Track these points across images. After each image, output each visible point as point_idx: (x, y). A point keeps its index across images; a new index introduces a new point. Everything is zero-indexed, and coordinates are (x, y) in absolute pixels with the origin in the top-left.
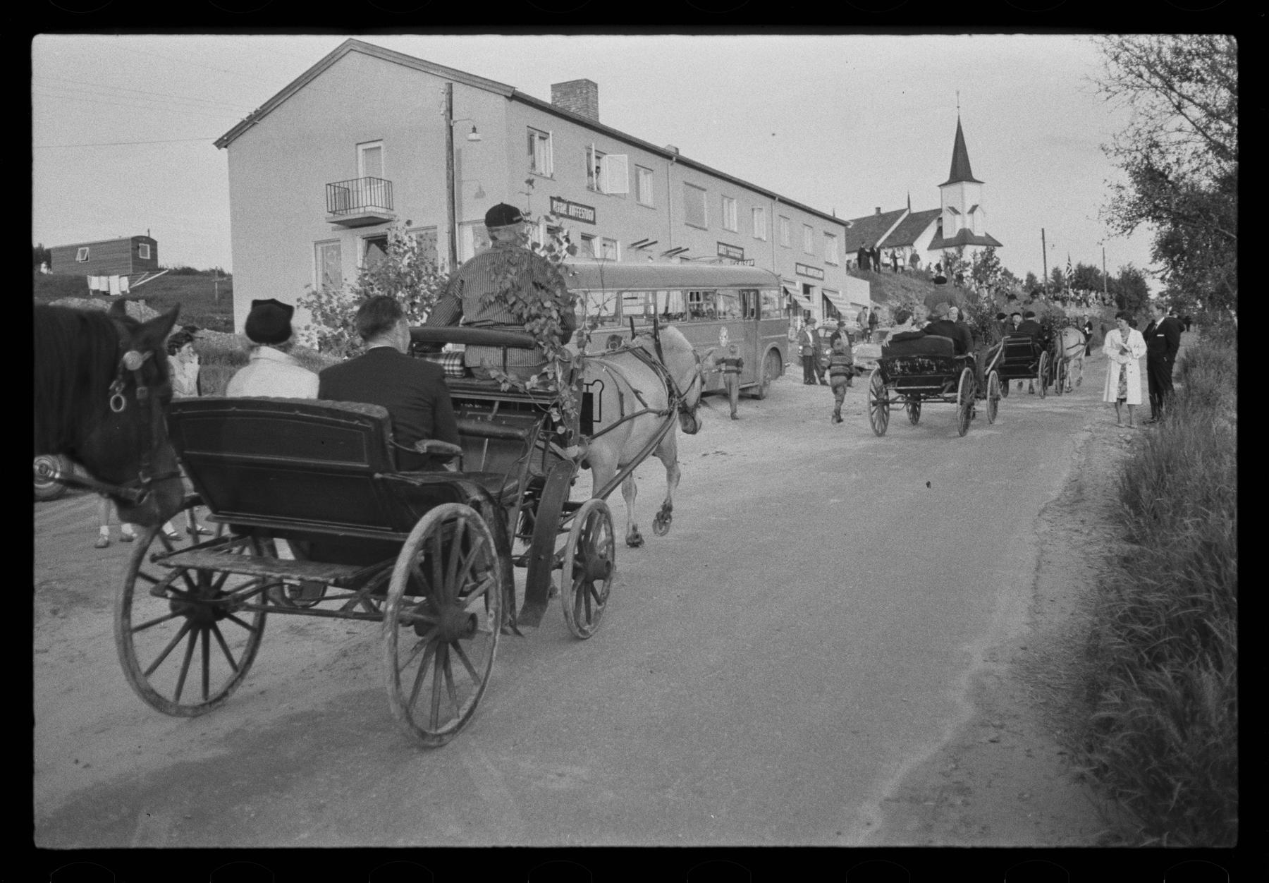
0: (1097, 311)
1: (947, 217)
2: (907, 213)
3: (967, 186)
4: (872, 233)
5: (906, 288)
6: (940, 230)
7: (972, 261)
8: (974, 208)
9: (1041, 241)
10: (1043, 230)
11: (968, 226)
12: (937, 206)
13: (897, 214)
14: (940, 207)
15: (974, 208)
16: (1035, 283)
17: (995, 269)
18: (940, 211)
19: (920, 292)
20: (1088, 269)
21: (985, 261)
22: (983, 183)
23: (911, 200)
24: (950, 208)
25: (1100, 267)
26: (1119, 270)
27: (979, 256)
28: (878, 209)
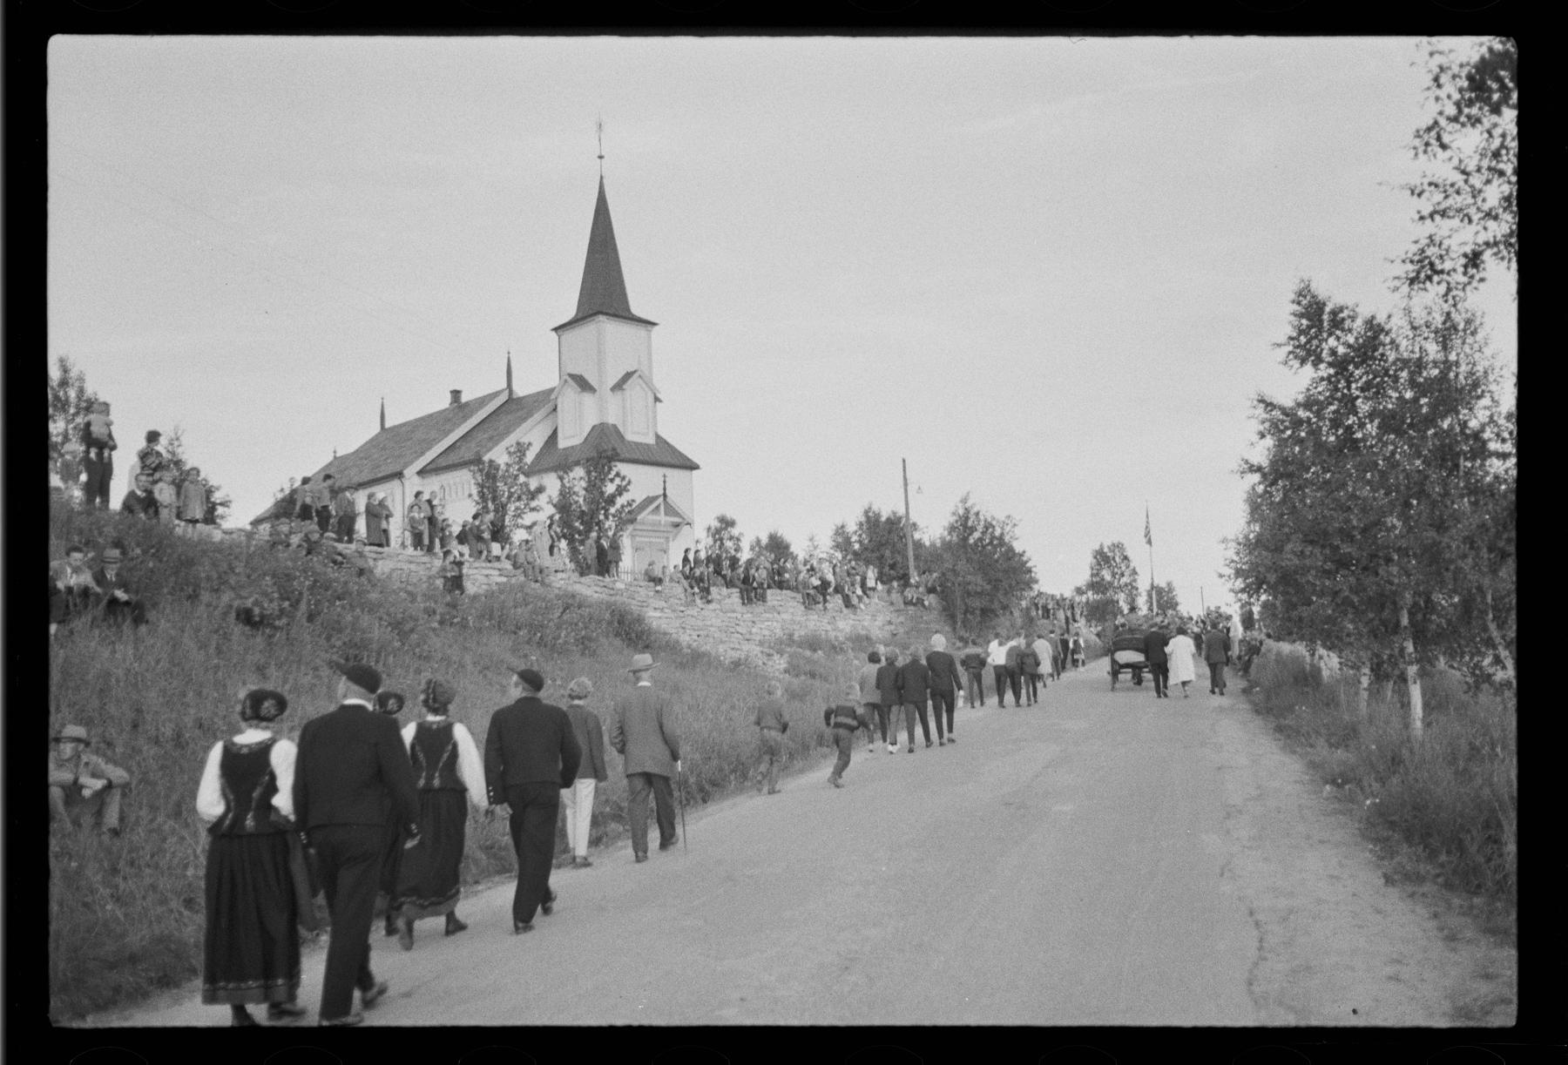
0: (880, 620)
1: (569, 399)
2: (504, 398)
3: (610, 329)
10: (904, 461)
11: (611, 420)
22: (654, 324)
23: (513, 365)
24: (571, 376)
28: (456, 394)
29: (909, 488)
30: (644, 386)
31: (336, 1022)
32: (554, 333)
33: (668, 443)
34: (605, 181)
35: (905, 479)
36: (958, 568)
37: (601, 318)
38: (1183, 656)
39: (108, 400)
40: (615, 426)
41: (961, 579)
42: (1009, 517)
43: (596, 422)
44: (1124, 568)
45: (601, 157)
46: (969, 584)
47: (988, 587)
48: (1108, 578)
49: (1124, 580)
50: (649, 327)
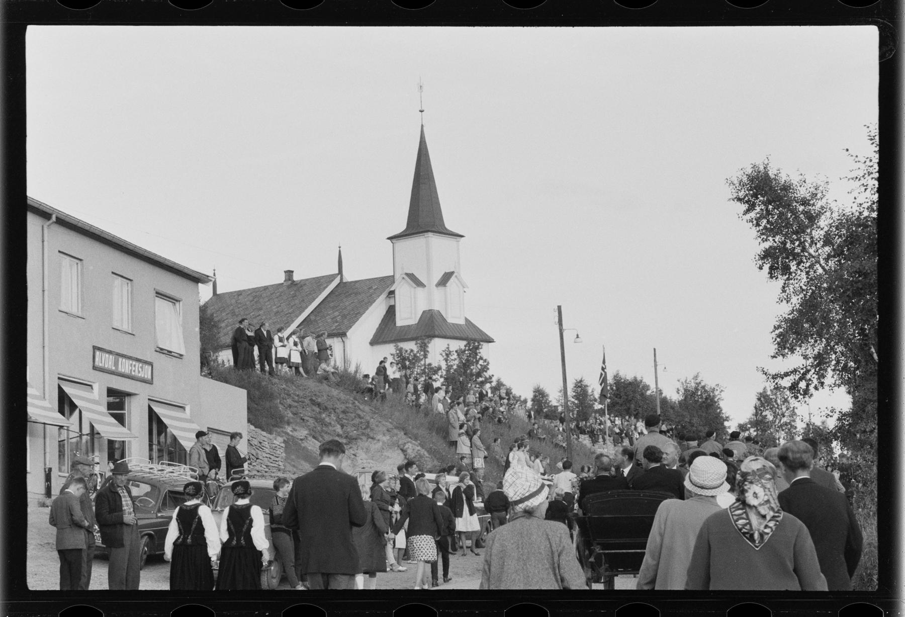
1: (403, 290)
2: (337, 281)
3: (434, 240)
5: (319, 405)
6: (391, 311)
7: (444, 366)
9: (557, 327)
10: (655, 349)
11: (436, 307)
13: (319, 283)
17: (480, 379)
18: (390, 280)
19: (344, 412)
20: (630, 383)
21: (465, 366)
22: (462, 236)
24: (407, 274)
25: (649, 380)
26: (679, 385)
27: (455, 356)
28: (289, 273)
29: (658, 367)
32: (389, 241)
34: (425, 128)
35: (655, 361)
37: (430, 234)
40: (439, 311)
42: (718, 385)
43: (427, 309)
44: (784, 409)
45: (421, 111)
48: (770, 418)
49: (784, 420)
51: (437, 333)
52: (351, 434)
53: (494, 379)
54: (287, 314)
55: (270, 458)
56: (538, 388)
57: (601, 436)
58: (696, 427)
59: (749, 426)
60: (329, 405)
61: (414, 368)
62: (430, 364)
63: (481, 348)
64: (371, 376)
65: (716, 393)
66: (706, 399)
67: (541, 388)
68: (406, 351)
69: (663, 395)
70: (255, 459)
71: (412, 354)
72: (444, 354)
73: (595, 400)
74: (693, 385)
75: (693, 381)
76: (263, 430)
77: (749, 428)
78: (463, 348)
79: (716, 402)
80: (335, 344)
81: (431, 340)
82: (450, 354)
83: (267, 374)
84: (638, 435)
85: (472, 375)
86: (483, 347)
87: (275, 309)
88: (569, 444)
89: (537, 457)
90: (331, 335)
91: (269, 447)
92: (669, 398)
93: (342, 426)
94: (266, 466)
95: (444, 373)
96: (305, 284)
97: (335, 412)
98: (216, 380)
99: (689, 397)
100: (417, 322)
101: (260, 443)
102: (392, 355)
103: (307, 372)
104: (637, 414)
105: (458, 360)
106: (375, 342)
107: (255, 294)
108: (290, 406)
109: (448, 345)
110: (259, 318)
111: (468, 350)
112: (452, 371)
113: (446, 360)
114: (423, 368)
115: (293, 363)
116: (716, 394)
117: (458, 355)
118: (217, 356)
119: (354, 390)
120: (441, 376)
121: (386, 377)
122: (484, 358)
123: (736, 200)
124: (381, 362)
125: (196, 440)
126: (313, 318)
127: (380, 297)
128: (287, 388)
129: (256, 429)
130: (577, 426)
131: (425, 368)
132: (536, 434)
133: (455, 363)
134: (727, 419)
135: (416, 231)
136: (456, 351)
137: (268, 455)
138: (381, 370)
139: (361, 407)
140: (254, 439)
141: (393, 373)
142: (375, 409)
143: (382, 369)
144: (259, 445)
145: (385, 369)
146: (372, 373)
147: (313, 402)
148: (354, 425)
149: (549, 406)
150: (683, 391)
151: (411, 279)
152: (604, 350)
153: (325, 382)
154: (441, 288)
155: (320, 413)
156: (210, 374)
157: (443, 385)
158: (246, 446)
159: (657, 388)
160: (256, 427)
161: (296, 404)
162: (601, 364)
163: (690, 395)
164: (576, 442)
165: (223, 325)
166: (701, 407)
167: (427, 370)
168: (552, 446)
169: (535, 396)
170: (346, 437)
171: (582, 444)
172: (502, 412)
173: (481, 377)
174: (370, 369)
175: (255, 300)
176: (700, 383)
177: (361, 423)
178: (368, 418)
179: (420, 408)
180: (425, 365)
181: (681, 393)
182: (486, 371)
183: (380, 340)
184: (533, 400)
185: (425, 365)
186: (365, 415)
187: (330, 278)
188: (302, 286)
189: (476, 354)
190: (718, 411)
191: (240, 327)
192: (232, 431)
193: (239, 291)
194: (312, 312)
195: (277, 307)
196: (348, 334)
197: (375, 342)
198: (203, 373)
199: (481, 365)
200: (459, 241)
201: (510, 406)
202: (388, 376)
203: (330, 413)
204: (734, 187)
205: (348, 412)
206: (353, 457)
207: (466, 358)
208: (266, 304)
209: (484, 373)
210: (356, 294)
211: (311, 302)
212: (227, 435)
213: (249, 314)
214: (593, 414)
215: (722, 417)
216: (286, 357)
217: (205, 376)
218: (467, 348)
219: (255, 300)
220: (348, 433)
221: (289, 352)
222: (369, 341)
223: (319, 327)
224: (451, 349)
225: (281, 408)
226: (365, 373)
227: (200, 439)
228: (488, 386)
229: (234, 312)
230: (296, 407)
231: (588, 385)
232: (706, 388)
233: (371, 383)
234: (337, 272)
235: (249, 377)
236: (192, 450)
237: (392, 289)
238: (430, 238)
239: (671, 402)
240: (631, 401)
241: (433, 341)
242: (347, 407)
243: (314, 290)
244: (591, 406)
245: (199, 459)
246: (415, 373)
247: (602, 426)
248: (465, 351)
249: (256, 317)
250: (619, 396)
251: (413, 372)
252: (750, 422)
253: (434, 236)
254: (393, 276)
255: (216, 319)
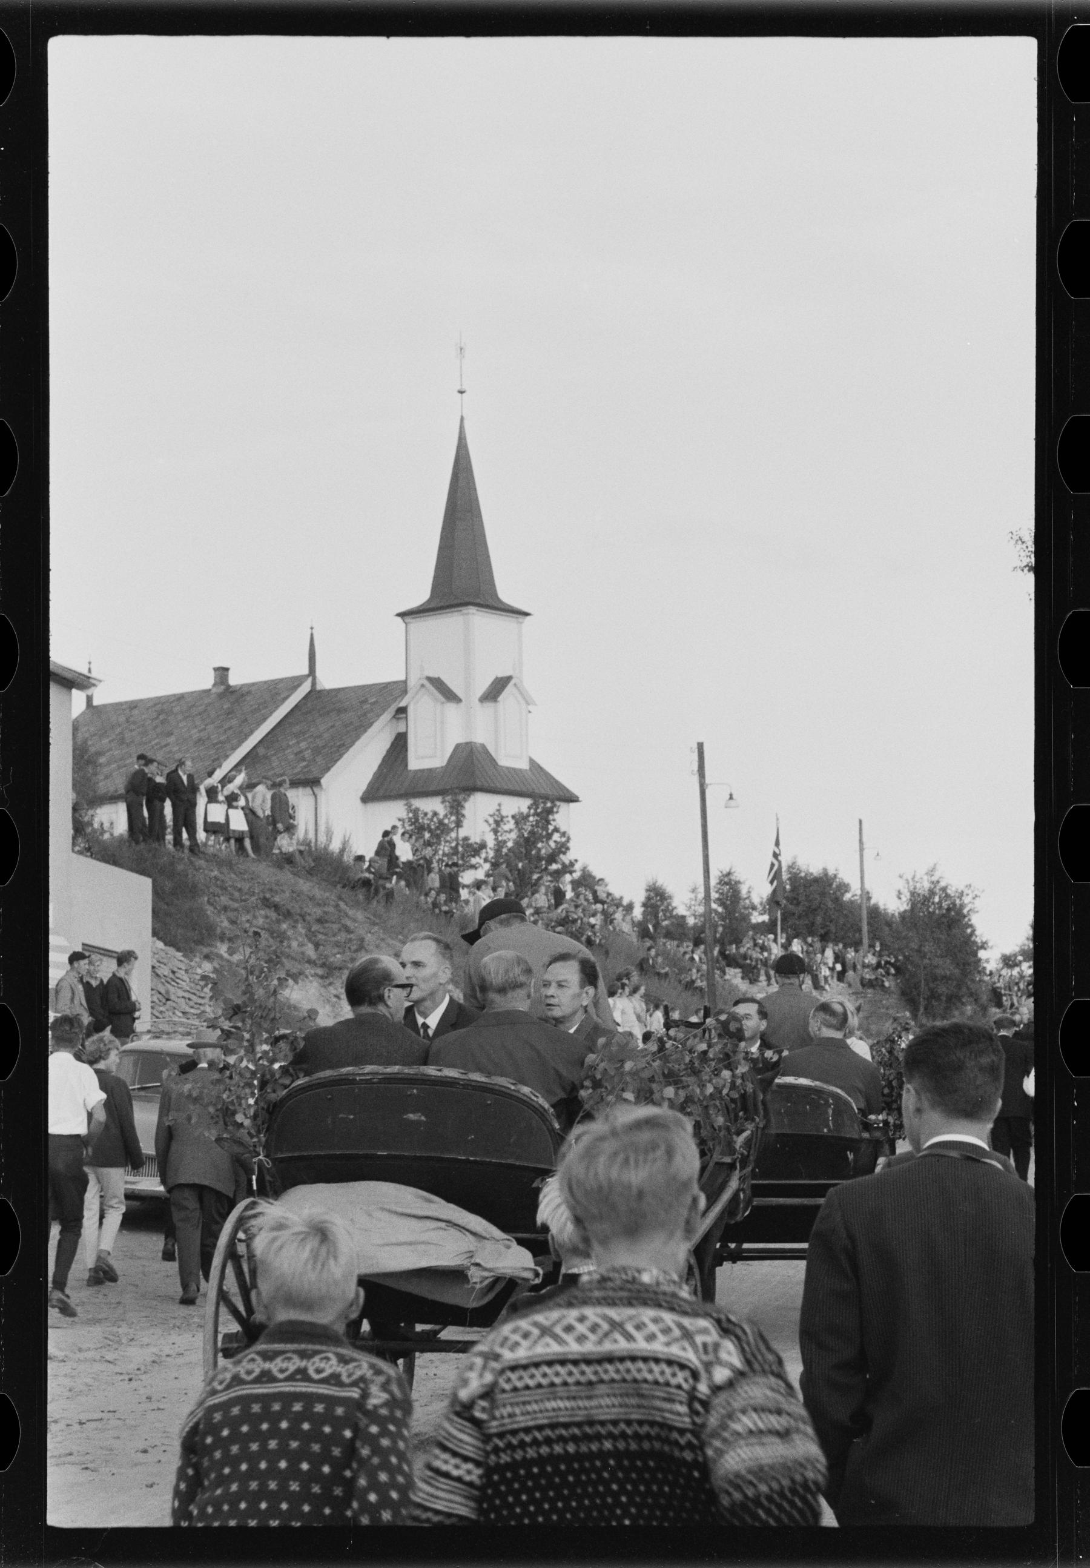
2: (306, 688)
3: (479, 620)
4: (200, 740)
5: (276, 907)
6: (400, 744)
7: (491, 842)
8: (497, 689)
9: (696, 779)
10: (860, 822)
11: (480, 737)
12: (394, 673)
13: (276, 690)
14: (403, 678)
15: (497, 689)
16: (669, 912)
17: (554, 867)
18: (400, 688)
19: (320, 921)
20: (816, 880)
21: (528, 842)
22: (527, 614)
24: (429, 679)
25: (848, 875)
26: (901, 885)
27: (510, 825)
28: (222, 672)
29: (865, 852)
30: (519, 696)
31: (508, 1303)
32: (399, 619)
33: (541, 768)
35: (861, 841)
36: (926, 949)
37: (472, 610)
38: (102, 1194)
39: (391, 826)
40: (483, 746)
41: (926, 961)
42: (969, 886)
45: (461, 392)
46: (936, 967)
47: (957, 971)
50: (521, 618)
51: (479, 783)
52: (331, 960)
53: (578, 867)
54: (217, 744)
55: (189, 999)
56: (654, 884)
57: (762, 972)
58: (930, 959)
59: (1020, 958)
60: (295, 908)
61: (439, 844)
62: (466, 839)
63: (557, 812)
64: (367, 859)
65: (966, 900)
66: (949, 910)
67: (659, 884)
68: (426, 814)
69: (873, 902)
70: (164, 1001)
71: (435, 819)
72: (491, 821)
73: (754, 908)
74: (927, 885)
75: (925, 877)
76: (178, 950)
77: (1020, 962)
78: (525, 810)
79: (965, 916)
80: (300, 799)
81: (469, 796)
82: (502, 820)
83: (186, 851)
84: (827, 970)
85: (539, 858)
86: (561, 810)
87: (195, 734)
88: (712, 985)
89: (657, 1007)
90: (295, 784)
91: (188, 980)
92: (882, 907)
93: (317, 945)
94: (183, 1013)
95: (491, 854)
96: (249, 692)
97: (304, 920)
98: (98, 859)
99: (919, 905)
100: (444, 764)
101: (173, 972)
102: (399, 820)
103: (256, 848)
104: (826, 933)
105: (516, 831)
106: (369, 797)
107: (159, 707)
108: (225, 909)
109: (499, 805)
110: (167, 749)
111: (533, 815)
112: (505, 850)
113: (495, 831)
114: (453, 844)
115: (234, 831)
116: (966, 901)
117: (517, 823)
118: (92, 816)
119: (339, 883)
120: (486, 860)
121: (393, 860)
122: (562, 830)
123: (1026, 570)
124: (386, 834)
125: (68, 967)
126: (261, 751)
127: (382, 717)
128: (221, 876)
129: (167, 948)
130: (722, 953)
131: (457, 844)
132: (653, 966)
133: (511, 838)
134: (983, 946)
135: (447, 604)
136: (513, 817)
137: (187, 995)
138: (386, 848)
139: (351, 913)
140: (162, 966)
141: (404, 852)
142: (375, 915)
143: (387, 845)
144: (171, 975)
145: (392, 845)
146: (369, 853)
147: (267, 903)
148: (337, 944)
149: (672, 916)
150: (908, 895)
151: (437, 688)
152: (777, 824)
153: (287, 866)
154: (489, 706)
155: (278, 921)
156: (89, 849)
157: (488, 875)
158: (149, 978)
159: (862, 888)
160: (166, 944)
161: (236, 905)
162: (772, 848)
163: (919, 902)
164: (719, 979)
165: (102, 760)
166: (939, 924)
167: (460, 849)
168: (680, 988)
169: (649, 898)
170: (323, 965)
171: (731, 985)
172: (593, 926)
173: (555, 862)
174: (366, 846)
175: (161, 717)
176: (938, 882)
177: (350, 940)
178: (361, 932)
179: (452, 916)
180: (457, 839)
181: (904, 899)
182: (564, 853)
183: (381, 793)
184: (644, 905)
185: (457, 839)
186: (356, 927)
187: (294, 683)
188: (243, 695)
189: (548, 822)
190: (969, 931)
191: (143, 770)
192: (120, 947)
193: (132, 702)
194: (260, 742)
195: (200, 731)
196: (323, 781)
197: (369, 797)
198: (77, 848)
199: (555, 842)
200: (521, 623)
201: (608, 918)
202: (397, 858)
203: (296, 921)
204: (1024, 546)
205: (327, 921)
206: (335, 1000)
207: (530, 828)
208: (180, 725)
209: (562, 856)
210: (339, 711)
211: (259, 724)
212: (111, 956)
213: (150, 742)
214: (751, 933)
215: (975, 943)
216: (223, 821)
217: (80, 853)
218: (532, 811)
219: (161, 717)
220: (326, 957)
221: (225, 813)
222: (360, 794)
223: (273, 768)
224: (504, 813)
225: (209, 910)
226: (359, 853)
227: (76, 964)
228: (568, 878)
229: (123, 738)
230: (236, 910)
231: (742, 880)
232: (949, 891)
233: (368, 870)
234: (306, 671)
235: (154, 856)
236: (62, 984)
237: (402, 704)
238: (470, 616)
239: (886, 914)
240: (815, 910)
241: (472, 797)
242: (326, 913)
243: (265, 702)
244: (746, 918)
245: (72, 999)
246: (441, 852)
247: (766, 954)
248: (528, 816)
249: (162, 748)
250: (795, 902)
251: (436, 852)
252: (1023, 952)
253: (480, 613)
254: (405, 682)
255: (92, 750)
